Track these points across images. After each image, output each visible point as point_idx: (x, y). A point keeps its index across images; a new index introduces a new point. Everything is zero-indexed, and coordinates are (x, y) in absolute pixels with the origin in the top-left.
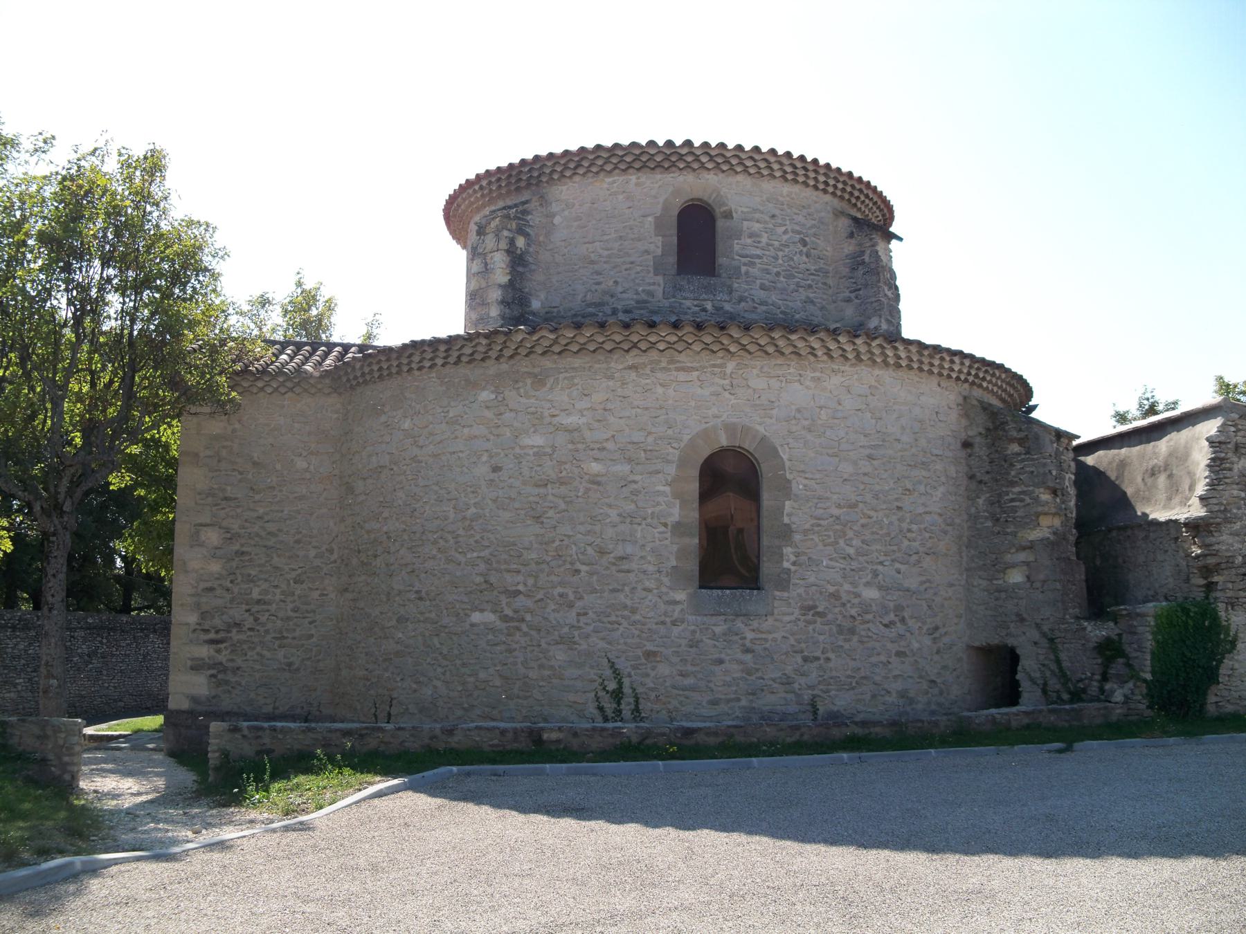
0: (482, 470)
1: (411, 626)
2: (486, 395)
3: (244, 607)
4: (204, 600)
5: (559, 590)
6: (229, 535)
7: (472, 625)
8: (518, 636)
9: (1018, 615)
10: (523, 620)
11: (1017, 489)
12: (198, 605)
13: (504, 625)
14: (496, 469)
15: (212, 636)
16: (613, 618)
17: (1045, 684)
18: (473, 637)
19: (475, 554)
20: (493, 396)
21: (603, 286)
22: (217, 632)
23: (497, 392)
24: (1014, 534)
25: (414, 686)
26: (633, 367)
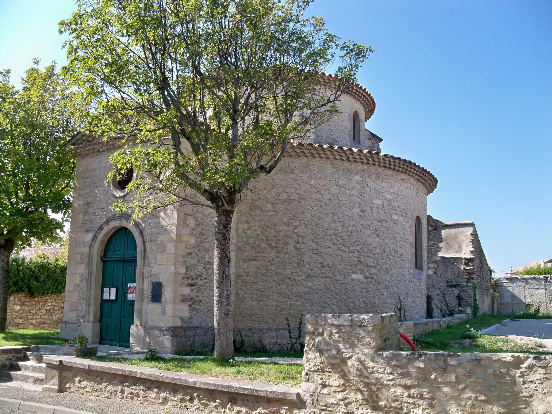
0: (357, 210)
1: (316, 280)
2: (357, 178)
3: (203, 266)
4: (188, 259)
5: (385, 266)
6: (198, 223)
7: (352, 280)
8: (371, 286)
9: (432, 285)
10: (373, 278)
11: (432, 242)
12: (185, 262)
13: (365, 280)
14: (363, 211)
15: (190, 281)
16: (399, 279)
17: (442, 308)
18: (353, 285)
19: (354, 248)
20: (361, 179)
21: (333, 137)
22: (193, 279)
23: (362, 176)
24: (432, 257)
25: (320, 308)
26: (403, 180)
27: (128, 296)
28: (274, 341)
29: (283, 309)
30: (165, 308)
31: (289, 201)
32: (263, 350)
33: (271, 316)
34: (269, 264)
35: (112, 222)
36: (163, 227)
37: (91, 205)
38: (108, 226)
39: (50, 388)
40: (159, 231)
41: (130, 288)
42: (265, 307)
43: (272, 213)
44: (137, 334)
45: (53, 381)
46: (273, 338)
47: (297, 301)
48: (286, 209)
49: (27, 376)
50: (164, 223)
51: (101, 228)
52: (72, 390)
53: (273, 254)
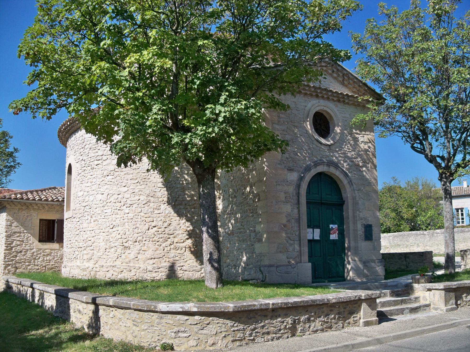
27: (331, 236)
38: (315, 169)
45: (451, 302)
49: (402, 309)
51: (308, 169)
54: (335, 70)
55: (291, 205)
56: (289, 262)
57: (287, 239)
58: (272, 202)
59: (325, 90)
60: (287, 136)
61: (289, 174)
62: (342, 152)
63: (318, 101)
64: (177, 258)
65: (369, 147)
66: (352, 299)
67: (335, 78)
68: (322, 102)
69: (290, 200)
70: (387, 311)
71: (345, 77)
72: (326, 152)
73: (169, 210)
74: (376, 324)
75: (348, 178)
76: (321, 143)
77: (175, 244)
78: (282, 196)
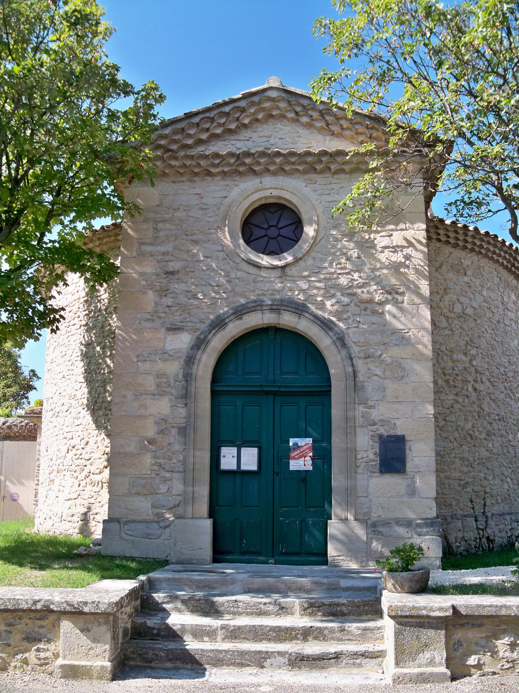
28: (460, 535)
29: (466, 483)
30: (415, 482)
31: (463, 316)
32: (449, 551)
33: (454, 496)
34: (448, 412)
35: (253, 314)
36: (395, 332)
37: (180, 275)
38: (238, 323)
39: (421, 674)
40: (386, 340)
41: (297, 446)
42: (447, 482)
43: (447, 332)
44: (345, 534)
46: (459, 530)
47: (480, 472)
48: (461, 328)
49: (260, 652)
50: (399, 326)
52: (486, 669)
53: (451, 397)
54: (298, 109)
55: (171, 400)
56: (160, 515)
57: (155, 467)
58: (124, 396)
59: (263, 154)
60: (170, 264)
61: (169, 338)
62: (322, 276)
63: (258, 180)
64: (92, 500)
65: (408, 257)
66: (25, 606)
67: (309, 126)
68: (268, 181)
69: (169, 389)
70: (203, 650)
71: (328, 118)
72: (273, 282)
73: (87, 418)
74: (101, 678)
75: (331, 334)
76: (258, 267)
77: (92, 476)
78: (150, 384)
